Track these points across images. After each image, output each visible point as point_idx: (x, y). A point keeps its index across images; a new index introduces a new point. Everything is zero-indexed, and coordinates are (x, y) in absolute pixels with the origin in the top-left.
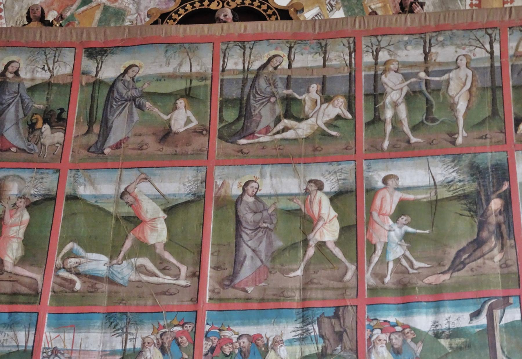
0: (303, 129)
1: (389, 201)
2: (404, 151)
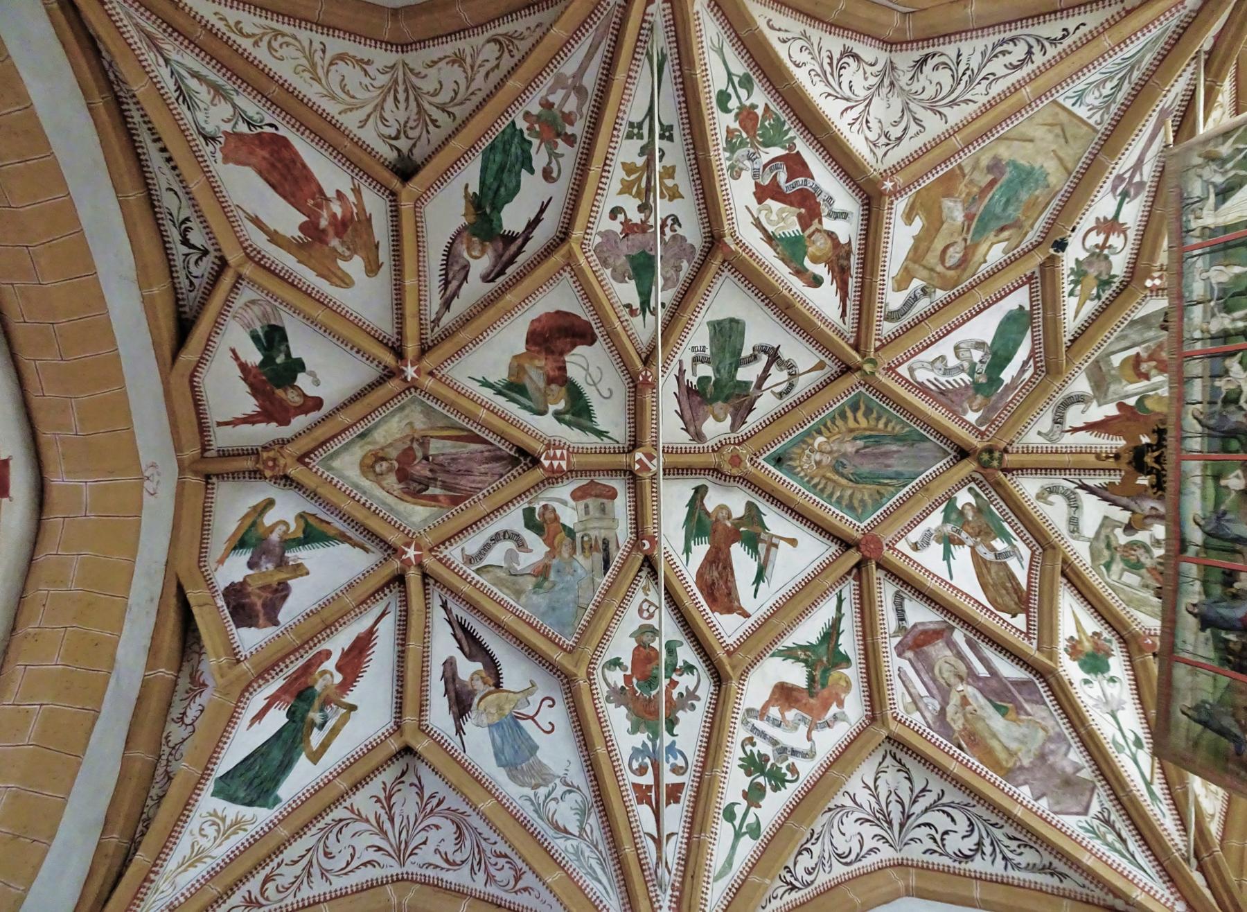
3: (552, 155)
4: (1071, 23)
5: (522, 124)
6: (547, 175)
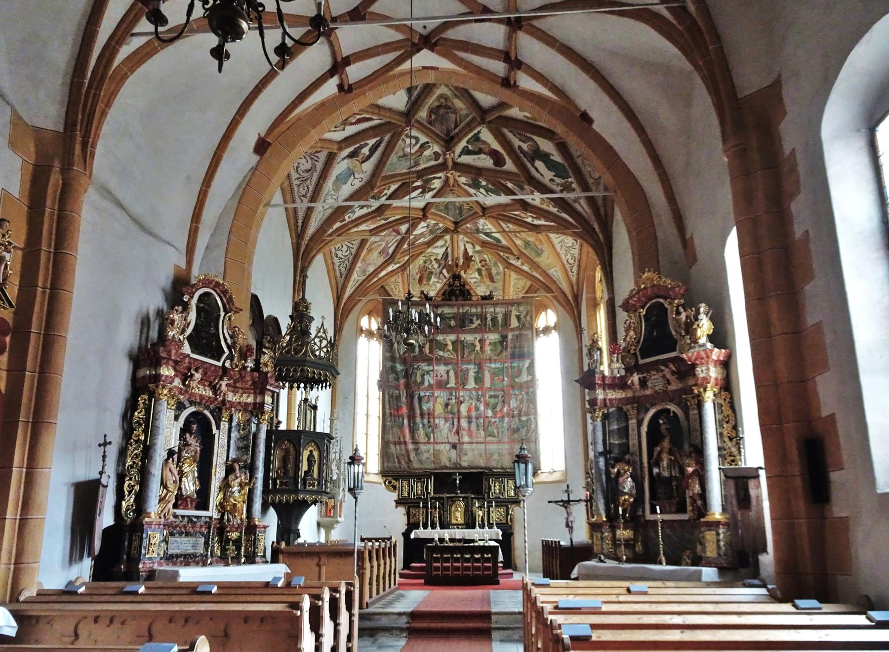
0: (473, 326)
1: (488, 342)
2: (490, 331)
3: (558, 185)
4: (575, 274)
5: (570, 180)
6: (552, 180)
